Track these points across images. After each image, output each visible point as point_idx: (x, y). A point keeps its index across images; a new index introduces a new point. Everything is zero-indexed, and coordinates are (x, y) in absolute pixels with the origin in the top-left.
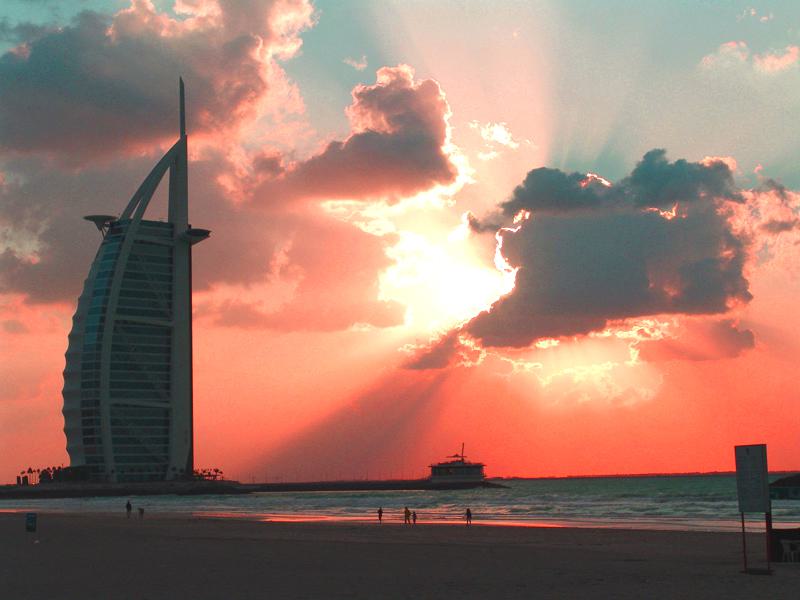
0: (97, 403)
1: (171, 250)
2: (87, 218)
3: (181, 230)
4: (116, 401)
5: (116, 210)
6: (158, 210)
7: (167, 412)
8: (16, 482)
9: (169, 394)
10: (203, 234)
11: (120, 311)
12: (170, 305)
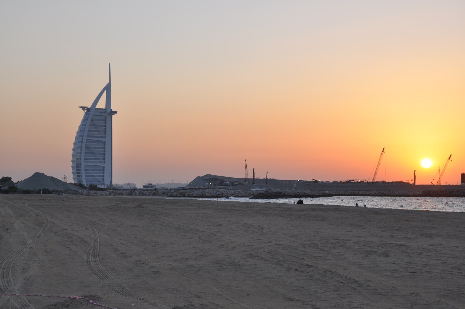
0: (81, 164)
1: (106, 117)
2: (414, 171)
3: (108, 111)
4: (86, 164)
5: (89, 106)
6: (101, 105)
7: (104, 167)
8: (355, 206)
9: (104, 162)
10: (115, 112)
11: (88, 136)
12: (105, 134)
